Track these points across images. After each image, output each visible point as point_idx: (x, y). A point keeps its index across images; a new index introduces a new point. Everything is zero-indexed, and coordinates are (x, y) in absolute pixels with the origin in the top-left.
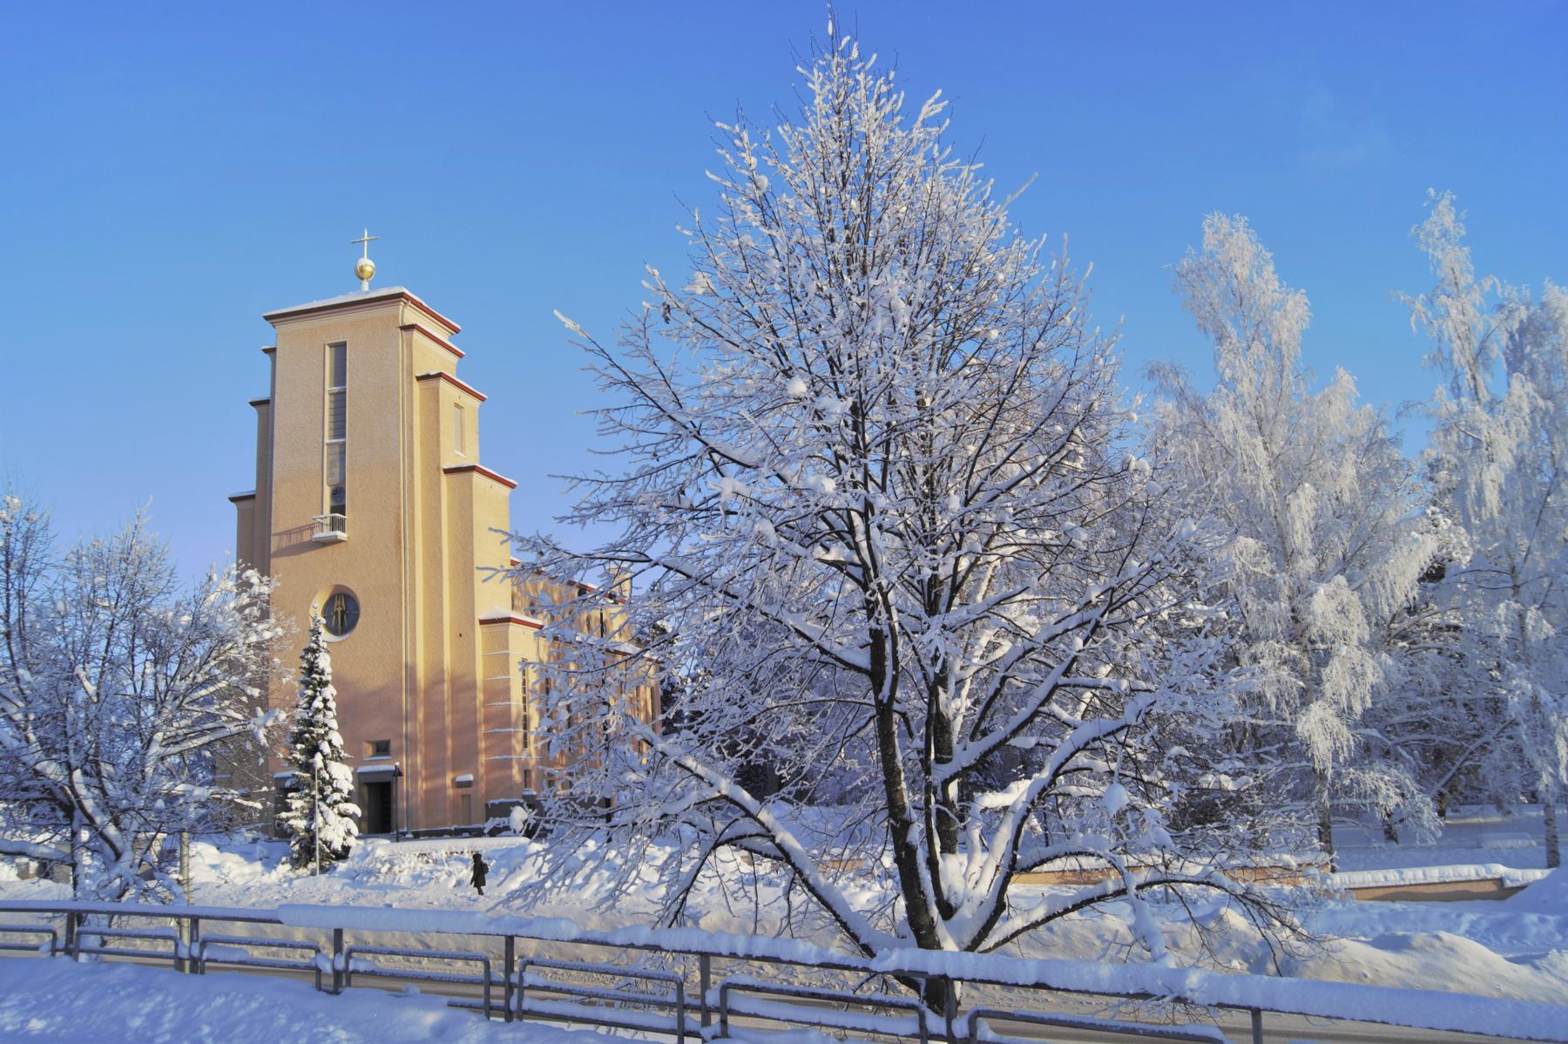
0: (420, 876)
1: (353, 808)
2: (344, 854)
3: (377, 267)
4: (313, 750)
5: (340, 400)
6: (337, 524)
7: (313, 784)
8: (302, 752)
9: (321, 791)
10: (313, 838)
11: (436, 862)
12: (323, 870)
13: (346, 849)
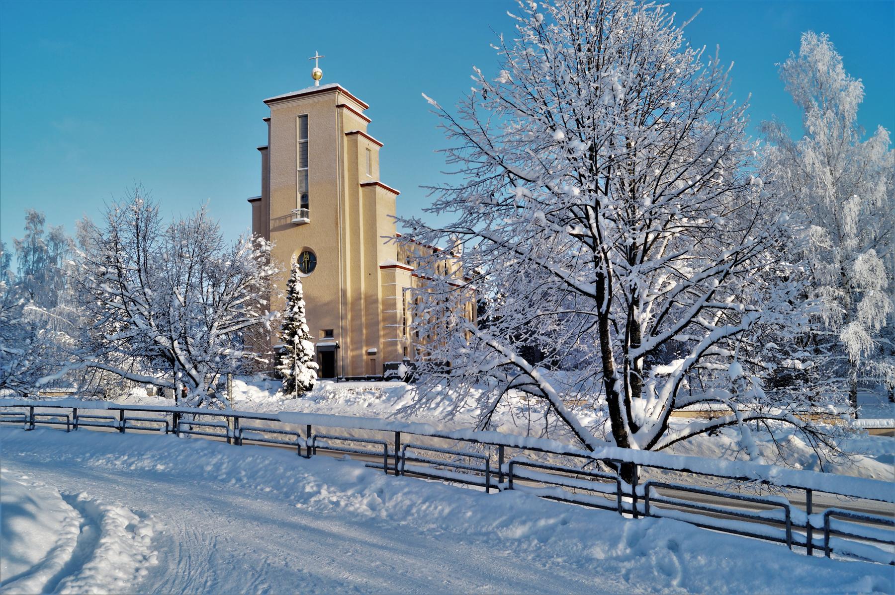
0: (349, 401)
1: (315, 365)
2: (310, 388)
4: (293, 334)
5: (305, 146)
6: (304, 214)
8: (288, 334)
9: (298, 355)
10: (294, 379)
11: (357, 393)
12: (299, 396)
13: (311, 386)
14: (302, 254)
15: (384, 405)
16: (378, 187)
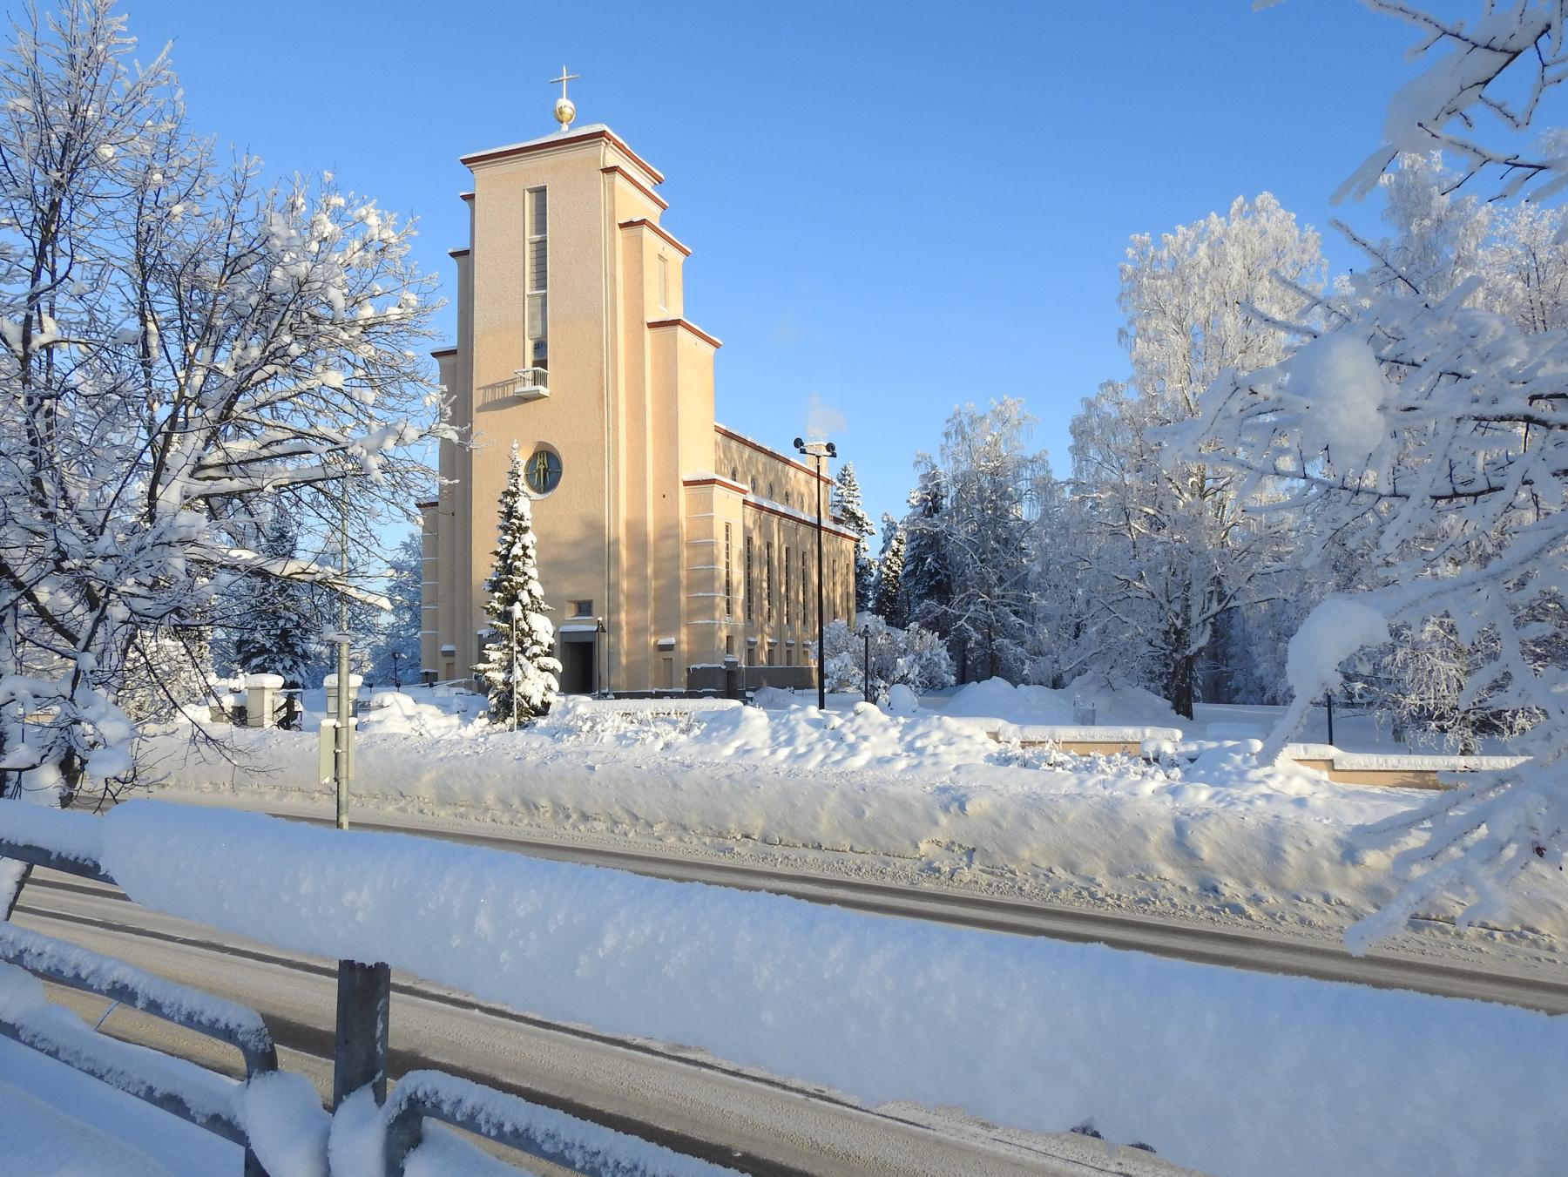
0: (624, 736)
1: (554, 663)
2: (543, 711)
3: (578, 110)
4: (512, 599)
5: (541, 248)
6: (539, 379)
7: (515, 638)
8: (501, 601)
9: (520, 643)
10: (511, 692)
11: (640, 722)
12: (521, 725)
14: (535, 455)
15: (696, 748)
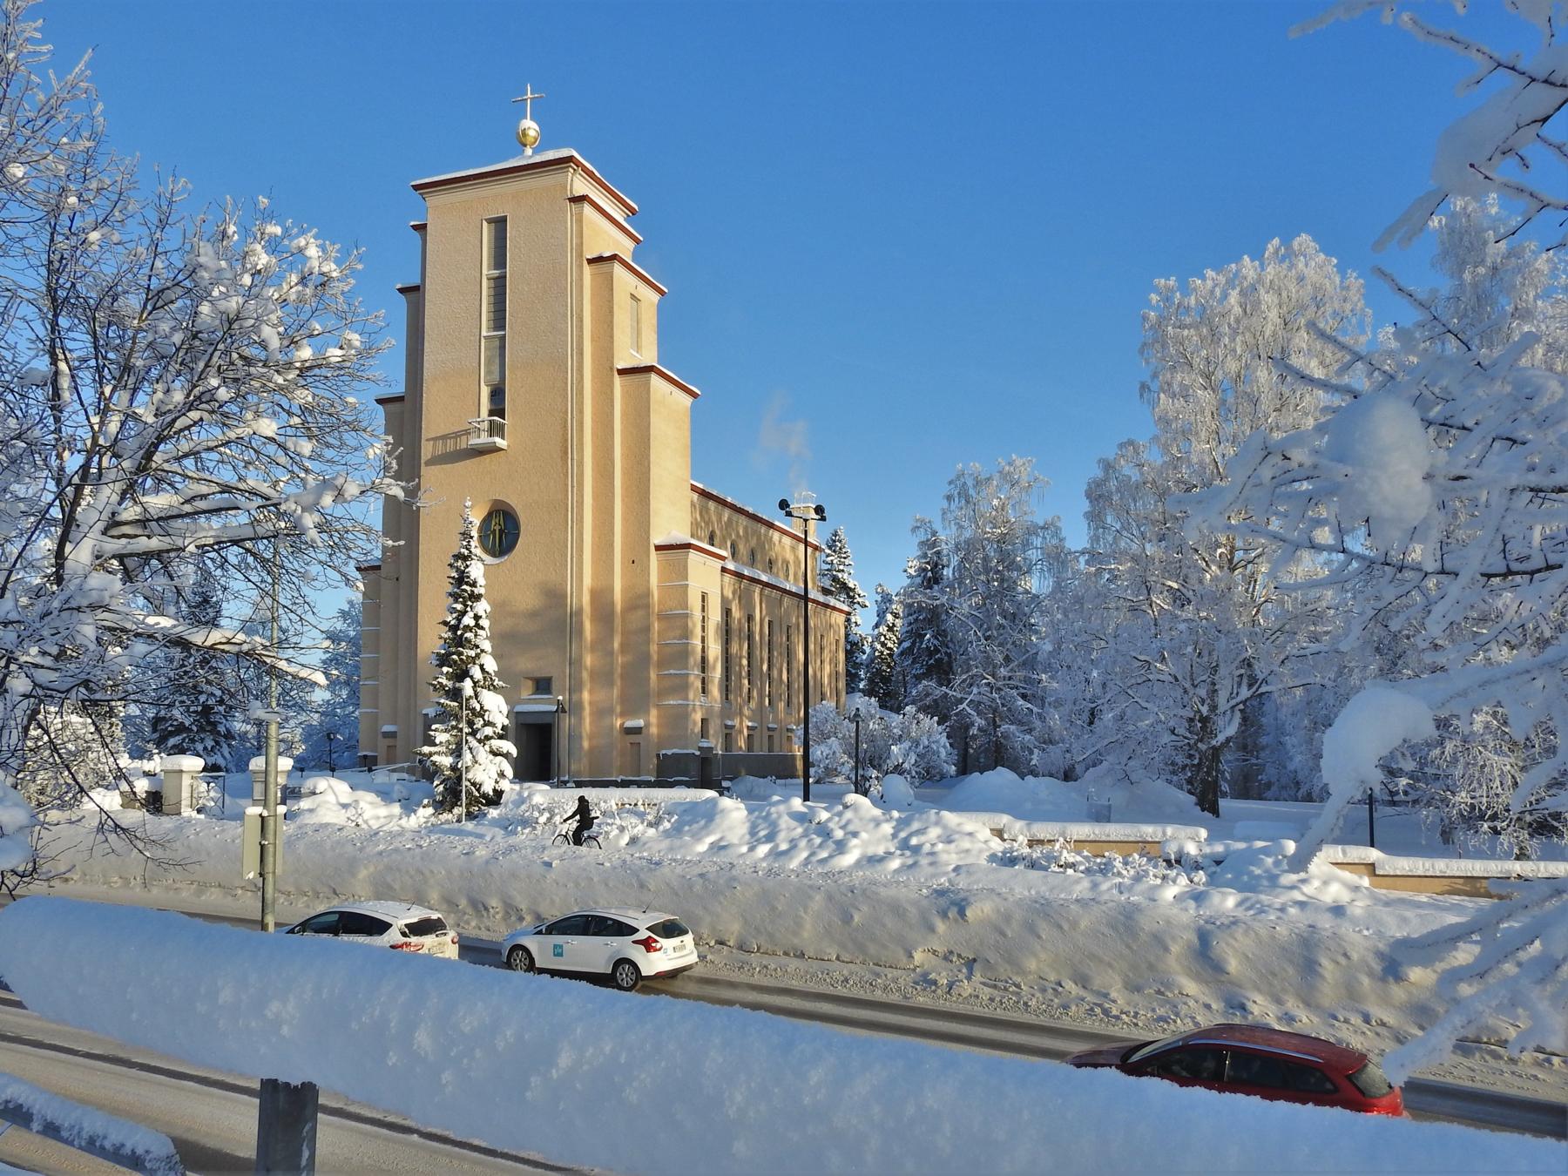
1: (508, 746)
4: (462, 674)
5: (499, 285)
6: (496, 430)
8: (449, 676)
9: (471, 723)
10: (459, 779)
12: (470, 816)
13: (499, 794)
14: (490, 515)
15: (666, 844)
16: (654, 378)
